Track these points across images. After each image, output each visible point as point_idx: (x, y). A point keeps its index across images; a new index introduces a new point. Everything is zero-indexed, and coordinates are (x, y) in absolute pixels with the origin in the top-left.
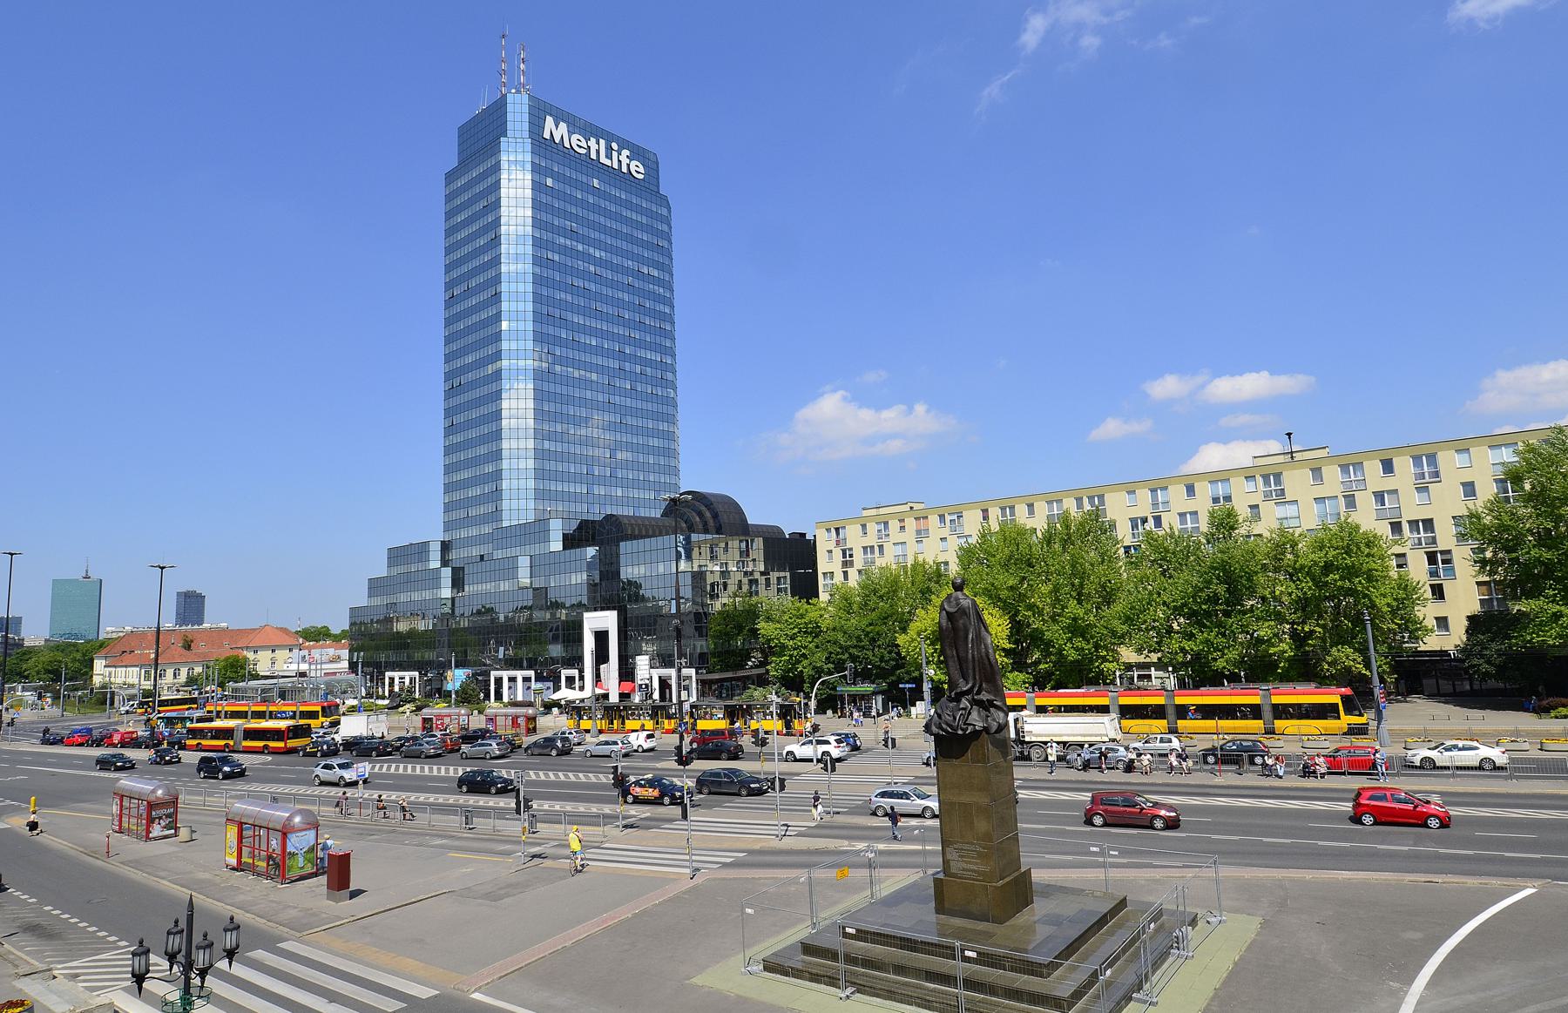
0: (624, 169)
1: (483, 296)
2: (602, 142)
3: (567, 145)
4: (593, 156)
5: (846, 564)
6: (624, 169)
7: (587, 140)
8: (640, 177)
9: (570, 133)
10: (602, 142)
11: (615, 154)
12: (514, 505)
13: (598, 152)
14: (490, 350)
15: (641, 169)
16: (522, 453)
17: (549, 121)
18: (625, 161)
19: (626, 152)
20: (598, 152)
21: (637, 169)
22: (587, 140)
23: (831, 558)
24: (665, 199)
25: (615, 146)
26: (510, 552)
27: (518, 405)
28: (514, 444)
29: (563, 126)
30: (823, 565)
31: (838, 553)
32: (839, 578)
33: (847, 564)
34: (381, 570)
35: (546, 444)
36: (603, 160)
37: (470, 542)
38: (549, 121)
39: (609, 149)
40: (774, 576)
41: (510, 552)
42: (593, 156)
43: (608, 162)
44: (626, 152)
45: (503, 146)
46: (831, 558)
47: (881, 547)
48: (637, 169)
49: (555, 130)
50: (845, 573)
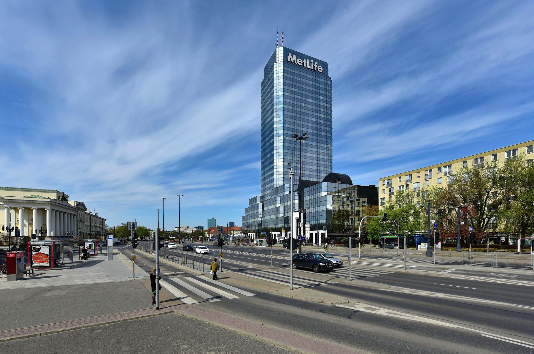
0: (316, 69)
1: (269, 155)
2: (308, 60)
3: (296, 63)
4: (305, 66)
5: (390, 194)
6: (316, 69)
7: (303, 60)
8: (321, 71)
9: (297, 59)
10: (308, 60)
11: (312, 64)
12: (278, 170)
13: (306, 64)
14: (271, 172)
15: (322, 69)
16: (280, 173)
17: (290, 55)
18: (316, 66)
19: (316, 63)
20: (306, 64)
21: (320, 68)
22: (303, 60)
23: (384, 193)
24: (330, 78)
25: (312, 61)
26: (275, 196)
27: (279, 162)
28: (278, 132)
29: (294, 56)
30: (380, 195)
31: (387, 190)
32: (387, 199)
33: (391, 194)
34: (244, 214)
35: (287, 138)
36: (308, 67)
37: (267, 195)
38: (290, 55)
39: (310, 63)
40: (362, 200)
41: (275, 196)
42: (305, 66)
43: (310, 67)
44: (316, 63)
45: (275, 66)
46: (384, 193)
47: (407, 185)
48: (320, 68)
49: (292, 58)
50: (390, 197)
